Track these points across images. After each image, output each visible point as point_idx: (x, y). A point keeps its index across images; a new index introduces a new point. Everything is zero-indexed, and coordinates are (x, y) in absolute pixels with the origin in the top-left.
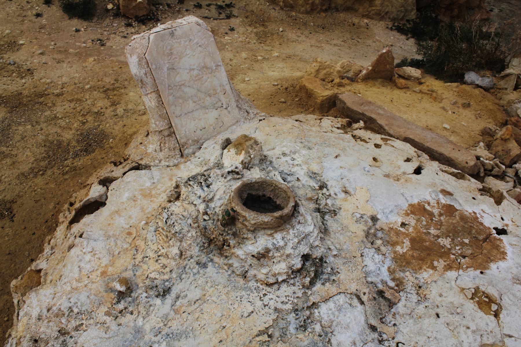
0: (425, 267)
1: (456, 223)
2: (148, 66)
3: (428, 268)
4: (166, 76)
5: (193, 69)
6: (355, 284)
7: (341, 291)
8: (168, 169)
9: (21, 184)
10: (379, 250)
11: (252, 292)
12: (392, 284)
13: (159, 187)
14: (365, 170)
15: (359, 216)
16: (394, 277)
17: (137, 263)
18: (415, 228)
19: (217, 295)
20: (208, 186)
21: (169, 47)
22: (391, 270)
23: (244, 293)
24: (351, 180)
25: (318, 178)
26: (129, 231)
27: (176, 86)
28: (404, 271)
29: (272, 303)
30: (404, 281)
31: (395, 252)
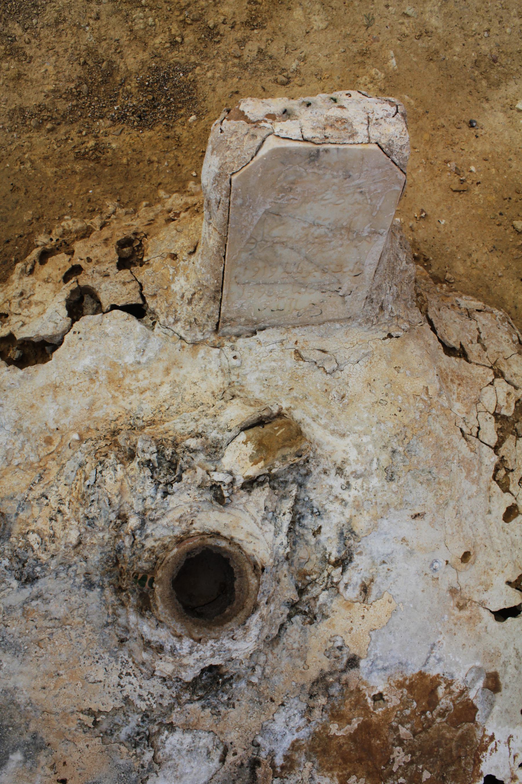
0: (335, 773)
1: (447, 739)
2: (228, 195)
3: (338, 776)
4: (255, 222)
5: (319, 226)
6: (237, 734)
7: (214, 729)
8: (179, 344)
9: (10, 131)
10: (310, 711)
11: (117, 661)
12: (279, 761)
13: (140, 376)
14: (432, 565)
15: (339, 644)
16: (291, 755)
17: (30, 498)
18: (387, 712)
19: (78, 632)
20: (166, 494)
21: (292, 178)
22: (297, 745)
23: (106, 656)
24: (393, 574)
25: (351, 542)
26: (51, 435)
27: (267, 242)
28: (308, 758)
29: (128, 687)
30: (296, 768)
31: (325, 728)
